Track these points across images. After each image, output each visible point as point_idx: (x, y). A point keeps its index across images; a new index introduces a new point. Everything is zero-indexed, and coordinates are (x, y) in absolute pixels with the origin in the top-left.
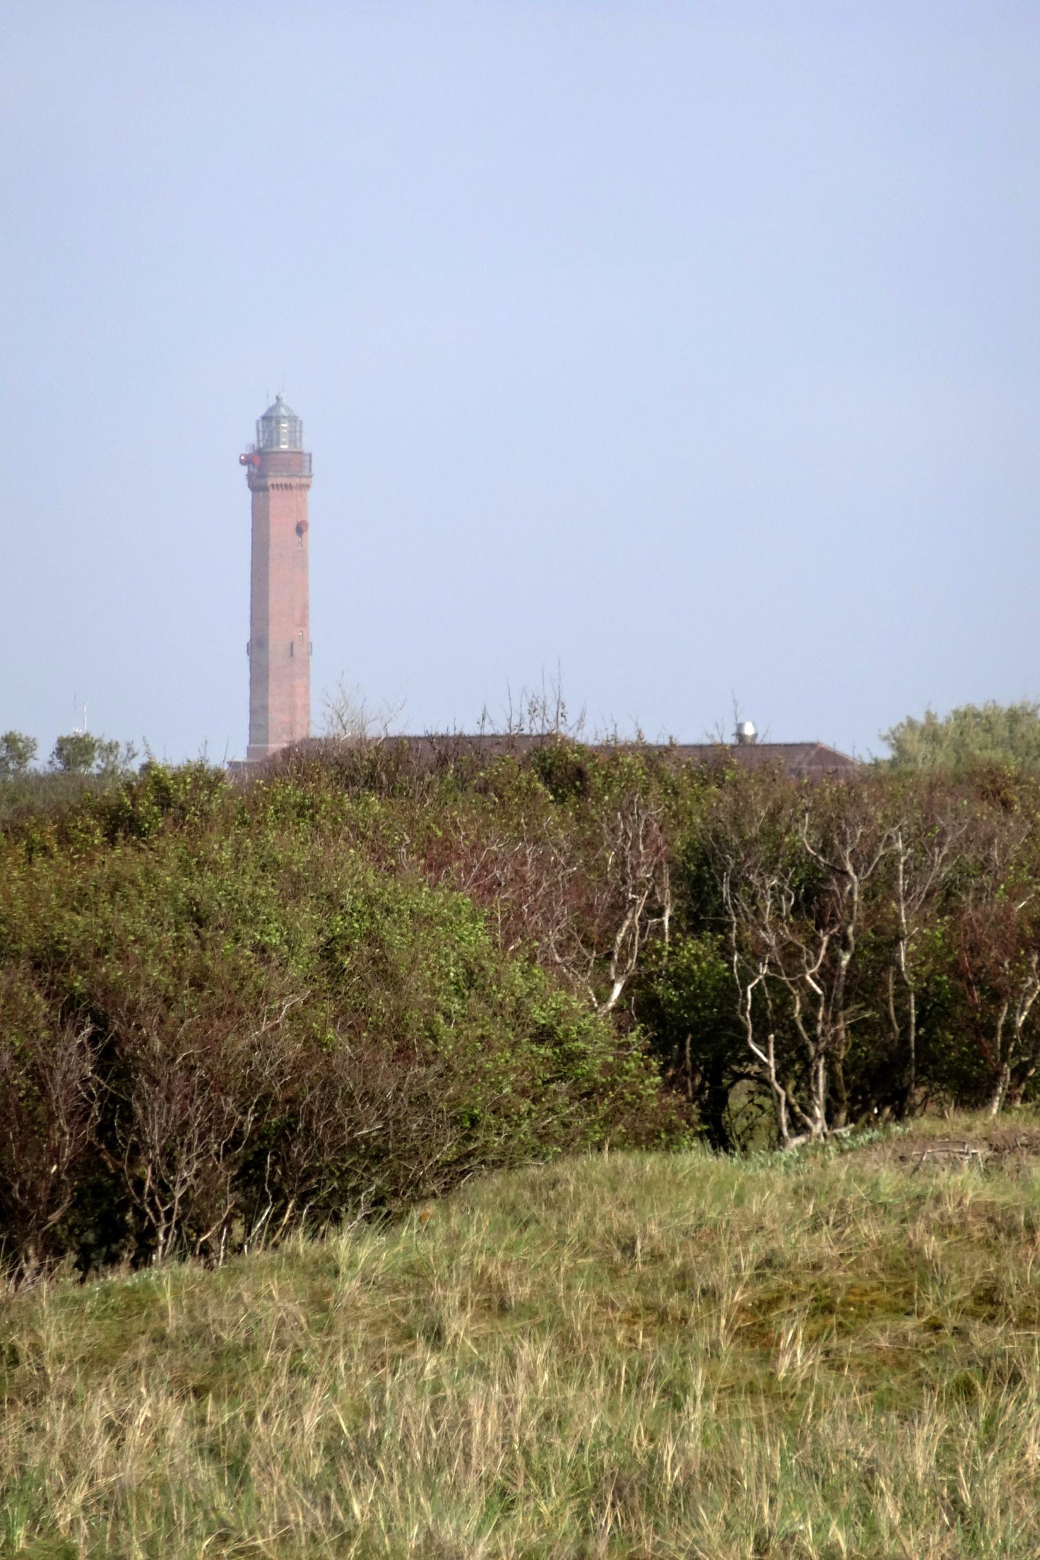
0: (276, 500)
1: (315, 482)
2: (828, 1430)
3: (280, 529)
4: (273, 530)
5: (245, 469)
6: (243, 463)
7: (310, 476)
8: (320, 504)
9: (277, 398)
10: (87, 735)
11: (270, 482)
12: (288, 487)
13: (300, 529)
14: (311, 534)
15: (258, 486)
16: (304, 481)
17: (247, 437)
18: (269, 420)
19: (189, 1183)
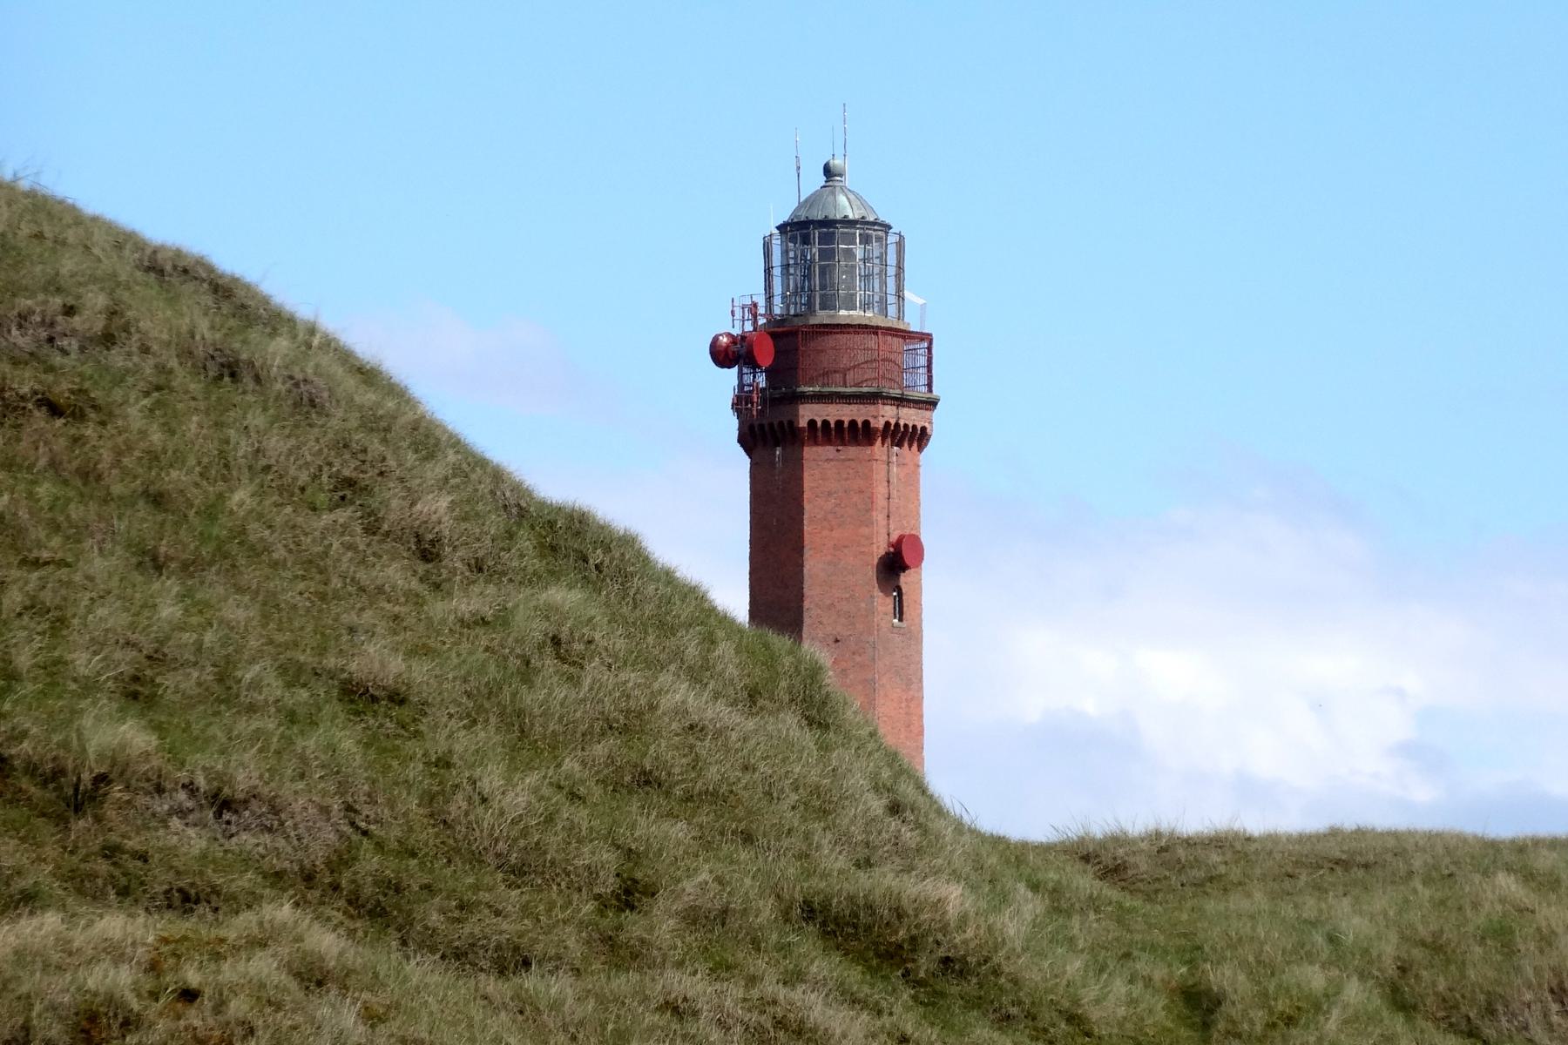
0: (821, 469)
1: (939, 423)
2: (1382, 901)
3: (833, 568)
4: (813, 565)
5: (729, 377)
6: (723, 355)
7: (932, 404)
8: (951, 487)
9: (828, 172)
10: (16, 179)
11: (807, 413)
12: (861, 434)
13: (896, 565)
14: (933, 584)
15: (769, 433)
16: (909, 416)
17: (734, 283)
18: (812, 238)
19: (198, 479)
